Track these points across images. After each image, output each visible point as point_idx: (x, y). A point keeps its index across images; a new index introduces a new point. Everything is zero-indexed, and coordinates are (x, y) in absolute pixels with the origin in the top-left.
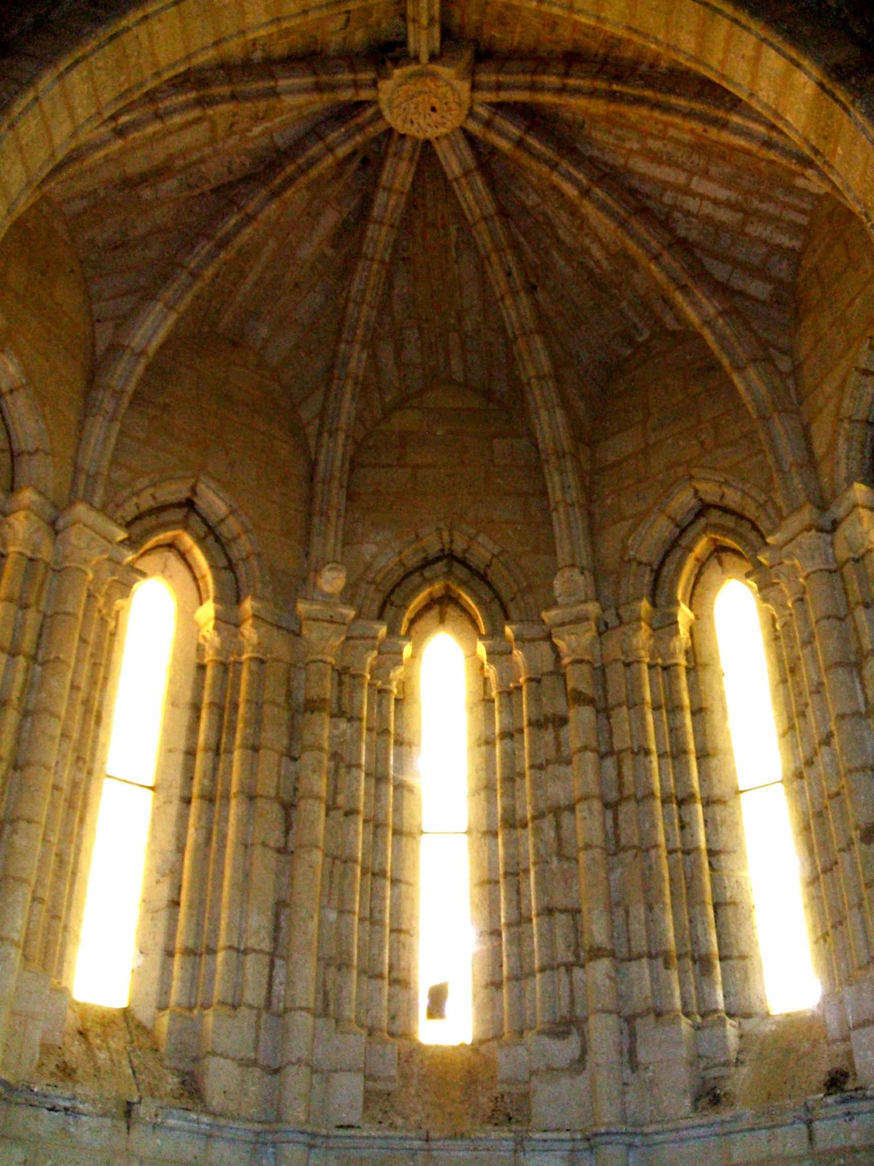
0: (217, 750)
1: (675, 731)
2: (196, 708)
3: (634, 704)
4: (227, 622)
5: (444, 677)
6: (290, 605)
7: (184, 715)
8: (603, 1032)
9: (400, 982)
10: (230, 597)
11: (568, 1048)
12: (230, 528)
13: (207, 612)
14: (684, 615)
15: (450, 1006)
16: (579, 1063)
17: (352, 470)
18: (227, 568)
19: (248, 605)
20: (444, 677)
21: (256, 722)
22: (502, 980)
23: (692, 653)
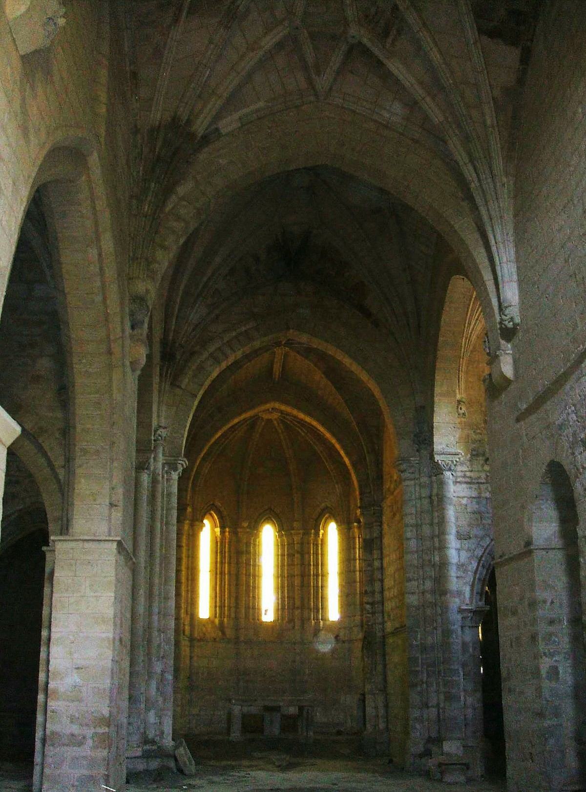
0: (222, 563)
1: (317, 559)
2: (217, 553)
3: (309, 553)
4: (223, 532)
5: (268, 537)
6: (236, 528)
7: (214, 555)
8: (298, 623)
9: (259, 609)
10: (223, 528)
11: (292, 624)
12: (222, 509)
13: (218, 530)
14: (322, 532)
15: (268, 613)
16: (294, 627)
17: (152, 99)
18: (221, 518)
19: (227, 529)
20: (268, 537)
21: (230, 557)
22: (281, 608)
23: (322, 540)
